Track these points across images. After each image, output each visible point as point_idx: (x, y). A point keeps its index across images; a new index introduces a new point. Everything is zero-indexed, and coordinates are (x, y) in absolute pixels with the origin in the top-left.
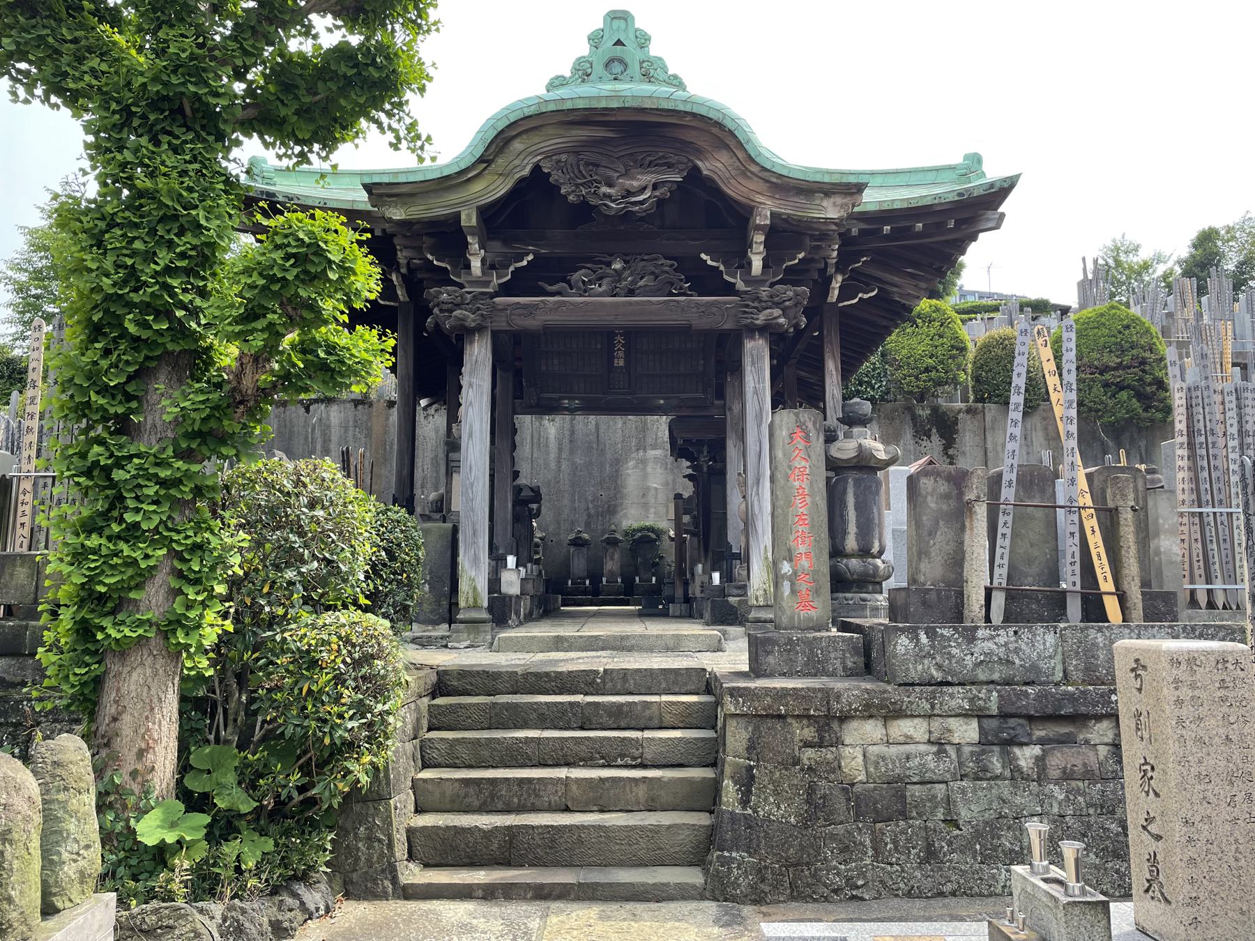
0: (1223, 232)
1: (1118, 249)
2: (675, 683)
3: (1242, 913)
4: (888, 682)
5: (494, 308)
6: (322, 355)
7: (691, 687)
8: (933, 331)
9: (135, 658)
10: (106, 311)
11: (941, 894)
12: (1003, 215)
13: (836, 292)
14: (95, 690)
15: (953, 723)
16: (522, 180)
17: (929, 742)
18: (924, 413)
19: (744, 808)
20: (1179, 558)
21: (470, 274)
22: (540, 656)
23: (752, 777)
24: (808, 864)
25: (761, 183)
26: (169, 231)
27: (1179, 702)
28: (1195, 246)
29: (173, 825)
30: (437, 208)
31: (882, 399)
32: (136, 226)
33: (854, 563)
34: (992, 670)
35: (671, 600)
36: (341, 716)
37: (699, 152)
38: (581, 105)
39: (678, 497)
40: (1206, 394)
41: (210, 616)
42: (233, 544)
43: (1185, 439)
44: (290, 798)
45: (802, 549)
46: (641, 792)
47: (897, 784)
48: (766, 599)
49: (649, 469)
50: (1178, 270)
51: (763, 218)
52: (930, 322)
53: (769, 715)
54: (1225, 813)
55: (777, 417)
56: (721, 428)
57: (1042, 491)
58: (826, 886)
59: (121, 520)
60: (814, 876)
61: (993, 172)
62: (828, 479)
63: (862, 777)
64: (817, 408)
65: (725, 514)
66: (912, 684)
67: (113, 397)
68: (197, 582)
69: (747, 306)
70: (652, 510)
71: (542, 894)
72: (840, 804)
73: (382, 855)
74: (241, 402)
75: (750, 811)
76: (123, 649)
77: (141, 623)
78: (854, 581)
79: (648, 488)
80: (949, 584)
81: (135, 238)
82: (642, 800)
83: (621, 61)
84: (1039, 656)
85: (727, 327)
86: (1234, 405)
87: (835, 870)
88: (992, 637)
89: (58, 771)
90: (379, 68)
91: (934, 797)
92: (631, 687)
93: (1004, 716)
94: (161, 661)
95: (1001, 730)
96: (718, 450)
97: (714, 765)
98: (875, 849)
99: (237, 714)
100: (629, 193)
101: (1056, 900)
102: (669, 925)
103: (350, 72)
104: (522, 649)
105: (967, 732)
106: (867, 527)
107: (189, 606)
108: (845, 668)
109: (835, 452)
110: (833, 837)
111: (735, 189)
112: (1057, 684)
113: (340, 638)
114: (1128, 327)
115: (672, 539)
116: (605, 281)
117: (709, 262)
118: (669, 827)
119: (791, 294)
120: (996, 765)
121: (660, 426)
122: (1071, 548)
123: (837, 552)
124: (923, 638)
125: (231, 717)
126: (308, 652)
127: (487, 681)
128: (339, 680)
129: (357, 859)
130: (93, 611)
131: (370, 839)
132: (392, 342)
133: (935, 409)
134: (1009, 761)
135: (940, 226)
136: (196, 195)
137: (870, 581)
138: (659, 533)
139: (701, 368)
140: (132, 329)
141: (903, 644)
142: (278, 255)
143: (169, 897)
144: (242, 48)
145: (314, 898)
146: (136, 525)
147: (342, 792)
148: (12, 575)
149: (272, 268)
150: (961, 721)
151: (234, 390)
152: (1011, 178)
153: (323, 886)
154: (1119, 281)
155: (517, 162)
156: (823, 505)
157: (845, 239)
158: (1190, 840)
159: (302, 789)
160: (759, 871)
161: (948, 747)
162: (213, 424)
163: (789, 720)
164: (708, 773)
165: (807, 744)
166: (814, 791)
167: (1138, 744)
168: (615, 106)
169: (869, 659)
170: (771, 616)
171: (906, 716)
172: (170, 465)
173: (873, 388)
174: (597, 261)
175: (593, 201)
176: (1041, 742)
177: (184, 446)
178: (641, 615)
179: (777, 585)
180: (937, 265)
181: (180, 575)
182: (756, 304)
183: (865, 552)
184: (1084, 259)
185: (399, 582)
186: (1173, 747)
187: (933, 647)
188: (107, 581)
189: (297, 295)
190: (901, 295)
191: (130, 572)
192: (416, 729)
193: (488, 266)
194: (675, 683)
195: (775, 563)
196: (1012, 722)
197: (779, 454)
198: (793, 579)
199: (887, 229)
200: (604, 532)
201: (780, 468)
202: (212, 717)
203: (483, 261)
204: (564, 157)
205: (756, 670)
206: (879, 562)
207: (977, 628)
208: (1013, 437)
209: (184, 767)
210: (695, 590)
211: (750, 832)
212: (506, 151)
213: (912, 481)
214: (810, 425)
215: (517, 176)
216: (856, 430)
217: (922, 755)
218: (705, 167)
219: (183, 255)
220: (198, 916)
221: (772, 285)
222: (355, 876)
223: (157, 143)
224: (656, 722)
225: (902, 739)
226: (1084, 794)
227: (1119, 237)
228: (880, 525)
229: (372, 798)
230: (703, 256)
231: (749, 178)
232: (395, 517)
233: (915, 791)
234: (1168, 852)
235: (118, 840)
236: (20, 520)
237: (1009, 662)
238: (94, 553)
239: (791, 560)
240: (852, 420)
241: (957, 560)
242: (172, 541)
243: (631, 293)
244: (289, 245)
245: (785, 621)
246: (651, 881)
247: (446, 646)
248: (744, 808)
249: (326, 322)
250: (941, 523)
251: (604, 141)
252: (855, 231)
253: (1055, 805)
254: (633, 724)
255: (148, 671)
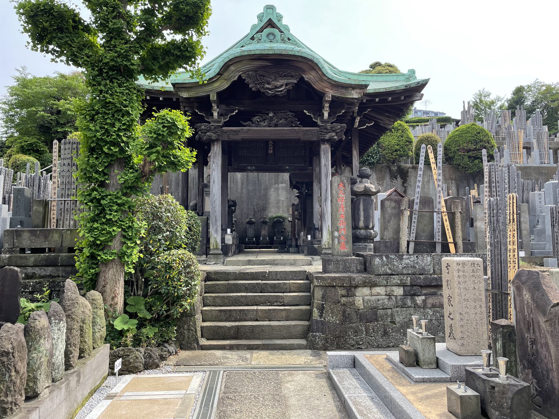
0: (526, 88)
1: (481, 95)
2: (295, 276)
3: (478, 342)
4: (372, 274)
5: (223, 132)
6: (172, 159)
7: (301, 278)
8: (398, 134)
9: (110, 266)
10: (97, 144)
11: (389, 347)
12: (423, 95)
13: (357, 124)
14: (96, 277)
15: (394, 288)
16: (234, 81)
17: (386, 295)
18: (394, 168)
19: (321, 318)
20: (484, 230)
21: (213, 118)
22: (243, 267)
23: (324, 307)
24: (343, 337)
25: (328, 84)
26: (118, 115)
27: (459, 277)
28: (514, 94)
29: (126, 323)
30: (201, 93)
31: (377, 162)
32: (108, 114)
33: (363, 232)
34: (408, 270)
35: (291, 246)
36: (181, 286)
37: (304, 71)
38: (257, 52)
39: (293, 205)
40: (496, 167)
41: (135, 251)
42: (141, 225)
43: (488, 185)
44: (163, 314)
45: (342, 227)
46: (284, 314)
47: (375, 309)
48: (328, 245)
49: (280, 192)
50: (506, 104)
51: (328, 98)
52: (397, 130)
53: (330, 286)
54: (473, 311)
55: (333, 178)
56: (311, 176)
57: (429, 206)
58: (349, 344)
59: (104, 217)
60: (345, 341)
61: (420, 77)
62: (352, 200)
63: (362, 307)
64: (350, 167)
65: (312, 212)
66: (380, 275)
67: (100, 174)
68: (130, 239)
69: (322, 131)
70: (281, 209)
71: (250, 348)
72: (354, 316)
73: (193, 335)
74: (144, 176)
75: (323, 319)
76: (106, 263)
77: (113, 254)
78: (362, 239)
79: (280, 200)
80: (395, 239)
81: (107, 118)
82: (284, 317)
83: (273, 34)
84: (425, 265)
85: (314, 139)
86: (507, 172)
87: (353, 339)
88: (409, 258)
89: (94, 302)
90: (189, 52)
91: (387, 314)
92: (279, 278)
93: (412, 286)
94: (119, 266)
95: (411, 290)
96: (310, 186)
97: (309, 305)
98: (366, 332)
99: (141, 286)
100: (276, 87)
101: (418, 337)
102: (295, 356)
103: (179, 54)
104: (236, 264)
105: (399, 291)
106: (368, 218)
107: (128, 248)
108: (357, 270)
109: (355, 189)
110: (351, 327)
111: (318, 86)
112: (431, 275)
113: (179, 259)
114: (479, 133)
115: (290, 221)
116: (266, 121)
117: (307, 114)
118: (294, 325)
119: (339, 127)
120: (409, 302)
121: (286, 176)
122: (437, 226)
123: (355, 227)
124: (384, 259)
125: (139, 287)
126: (169, 264)
127: (226, 276)
128: (180, 273)
129: (184, 337)
130: (95, 249)
131: (189, 329)
132: (196, 153)
133: (399, 167)
134: (414, 301)
135: (399, 98)
136: (128, 102)
137: (369, 238)
138: (284, 219)
139: (303, 154)
140: (106, 151)
141: (377, 261)
142: (160, 126)
143: (126, 345)
144: (141, 46)
145: (172, 348)
146: (111, 219)
147: (180, 312)
148: (52, 237)
149: (159, 130)
150: (397, 287)
151: (142, 172)
152: (426, 80)
153: (173, 345)
154: (481, 109)
155: (232, 75)
156: (350, 211)
157: (362, 103)
158: (461, 319)
159: (167, 311)
160: (326, 339)
161: (392, 297)
162: (135, 184)
163: (337, 288)
164: (308, 307)
165: (343, 296)
166: (345, 312)
167: (448, 291)
168: (271, 53)
169: (366, 267)
170: (331, 252)
171: (378, 286)
172: (121, 199)
173: (373, 158)
174: (262, 113)
175: (262, 90)
176: (425, 295)
177: (125, 191)
178: (278, 252)
179: (333, 240)
180: (397, 113)
181: (124, 237)
182: (325, 131)
183: (367, 227)
184: (464, 102)
185: (193, 239)
186: (457, 290)
187: (388, 262)
188: (101, 239)
189: (167, 140)
190: (384, 124)
191: (109, 236)
192: (201, 292)
193: (220, 115)
194: (295, 276)
195: (332, 232)
196: (415, 288)
197: (334, 192)
198: (339, 237)
199: (377, 100)
200: (261, 218)
201: (334, 197)
202: (132, 287)
203: (218, 113)
204: (250, 73)
205: (325, 271)
206: (372, 231)
207: (403, 255)
208: (418, 187)
209: (126, 304)
210: (300, 242)
211: (323, 326)
212: (228, 70)
213: (382, 202)
214: (345, 181)
215: (232, 80)
216: (364, 180)
217: (383, 300)
218: (306, 77)
219: (124, 124)
220: (137, 352)
221: (332, 123)
222: (184, 342)
223: (113, 83)
224: (288, 290)
225: (376, 294)
226: (439, 313)
227: (482, 89)
228: (373, 217)
229: (188, 315)
230: (305, 111)
231: (323, 82)
232: (191, 215)
233: (381, 312)
234: (455, 323)
235: (110, 327)
236: (52, 216)
237: (415, 267)
238: (96, 229)
239: (338, 231)
240: (363, 176)
241: (398, 231)
242: (122, 225)
243: (276, 126)
244: (165, 123)
245: (335, 253)
246: (288, 343)
247: (206, 264)
248: (321, 318)
249: (175, 149)
250: (392, 218)
251: (266, 67)
252: (364, 101)
253: (429, 316)
254: (280, 291)
255: (115, 270)
